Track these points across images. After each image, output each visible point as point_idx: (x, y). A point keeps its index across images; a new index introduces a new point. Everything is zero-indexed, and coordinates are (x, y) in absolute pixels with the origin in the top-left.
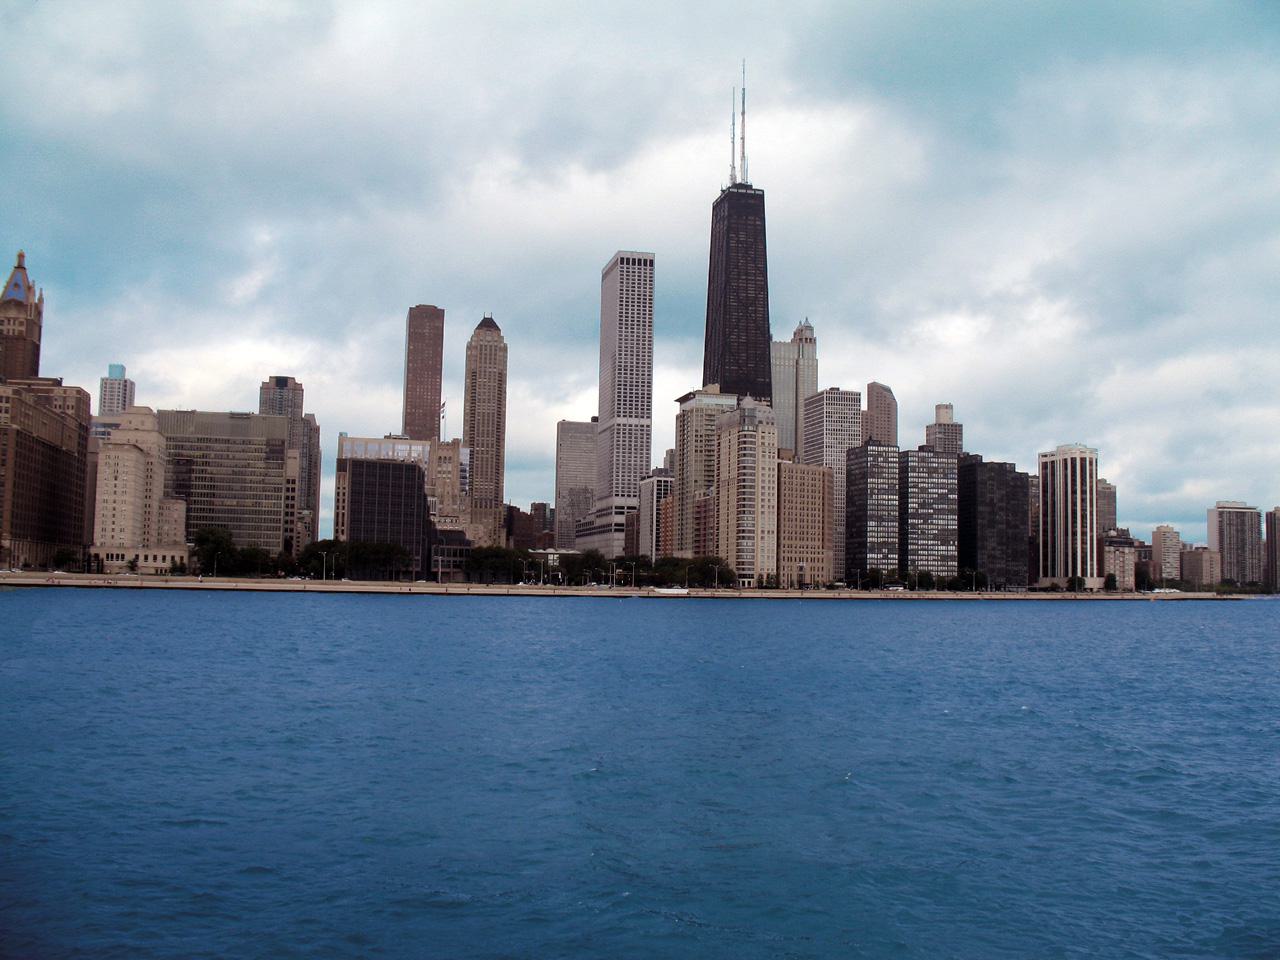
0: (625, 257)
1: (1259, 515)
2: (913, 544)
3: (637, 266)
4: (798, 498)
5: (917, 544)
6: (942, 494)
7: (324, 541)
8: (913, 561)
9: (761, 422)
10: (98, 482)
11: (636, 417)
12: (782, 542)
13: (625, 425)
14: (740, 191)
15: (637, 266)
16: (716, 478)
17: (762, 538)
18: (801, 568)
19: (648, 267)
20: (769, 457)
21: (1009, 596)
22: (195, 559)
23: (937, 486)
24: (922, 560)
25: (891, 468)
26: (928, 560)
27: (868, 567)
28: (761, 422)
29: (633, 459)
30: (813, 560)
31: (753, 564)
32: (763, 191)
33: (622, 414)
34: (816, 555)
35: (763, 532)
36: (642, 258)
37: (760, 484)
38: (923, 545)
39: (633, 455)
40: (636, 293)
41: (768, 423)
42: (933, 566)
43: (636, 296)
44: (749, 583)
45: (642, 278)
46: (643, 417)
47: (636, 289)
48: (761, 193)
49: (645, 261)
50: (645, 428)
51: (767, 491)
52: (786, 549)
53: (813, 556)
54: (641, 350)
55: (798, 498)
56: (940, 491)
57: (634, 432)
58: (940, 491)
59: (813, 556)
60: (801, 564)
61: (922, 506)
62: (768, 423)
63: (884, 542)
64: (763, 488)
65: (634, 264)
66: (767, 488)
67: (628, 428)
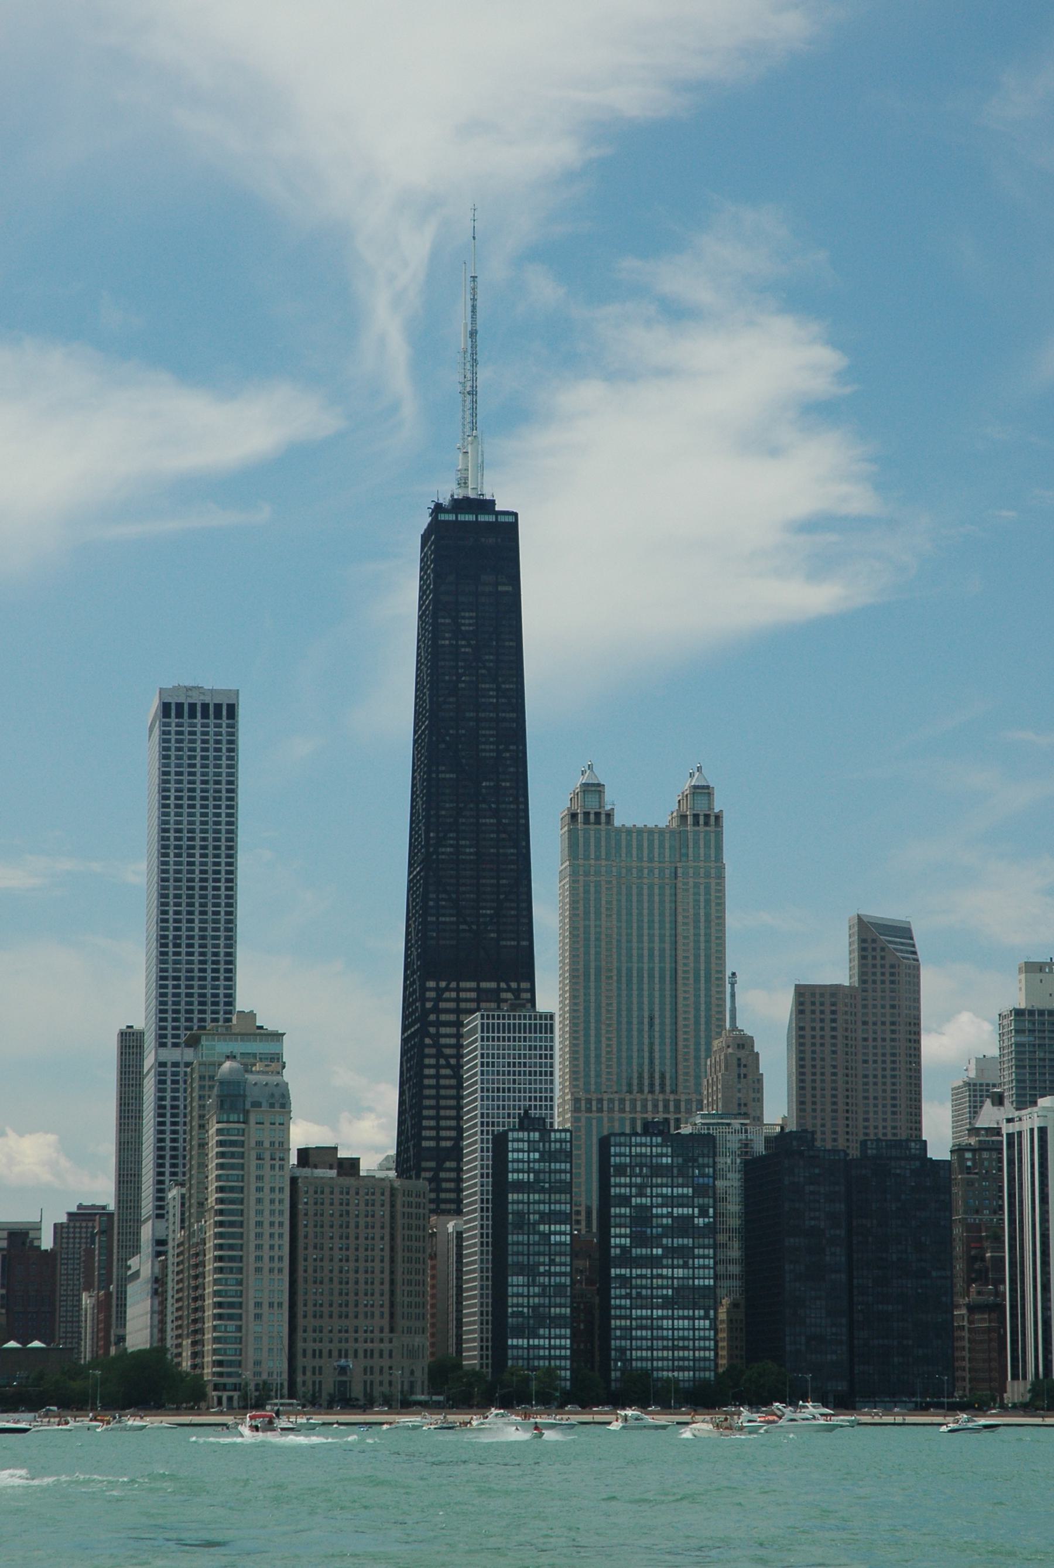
0: (173, 700)
2: (620, 1317)
3: (199, 720)
4: (336, 1240)
5: (630, 1318)
7: (791, 1132)
8: (622, 1350)
9: (257, 1104)
11: (175, 1045)
12: (301, 1322)
13: (175, 1064)
14: (462, 517)
15: (199, 720)
17: (258, 1316)
18: (343, 1370)
19: (224, 722)
20: (273, 1167)
21: (1038, 1421)
22: (618, 1251)
23: (671, 1201)
24: (638, 1349)
25: (556, 1171)
26: (652, 1349)
28: (257, 1104)
30: (369, 1354)
31: (239, 1364)
32: (516, 515)
33: (170, 1041)
34: (376, 1345)
35: (258, 1305)
36: (197, 699)
37: (253, 1219)
38: (641, 1318)
40: (198, 778)
41: (272, 1105)
42: (663, 1359)
44: (230, 1399)
45: (211, 745)
47: (198, 770)
48: (511, 519)
49: (218, 707)
51: (267, 1230)
52: (310, 1334)
53: (369, 1345)
54: (210, 901)
55: (336, 1240)
56: (677, 1211)
58: (677, 1211)
59: (369, 1345)
60: (343, 1362)
61: (639, 1240)
62: (272, 1105)
64: (259, 1224)
66: (266, 1224)
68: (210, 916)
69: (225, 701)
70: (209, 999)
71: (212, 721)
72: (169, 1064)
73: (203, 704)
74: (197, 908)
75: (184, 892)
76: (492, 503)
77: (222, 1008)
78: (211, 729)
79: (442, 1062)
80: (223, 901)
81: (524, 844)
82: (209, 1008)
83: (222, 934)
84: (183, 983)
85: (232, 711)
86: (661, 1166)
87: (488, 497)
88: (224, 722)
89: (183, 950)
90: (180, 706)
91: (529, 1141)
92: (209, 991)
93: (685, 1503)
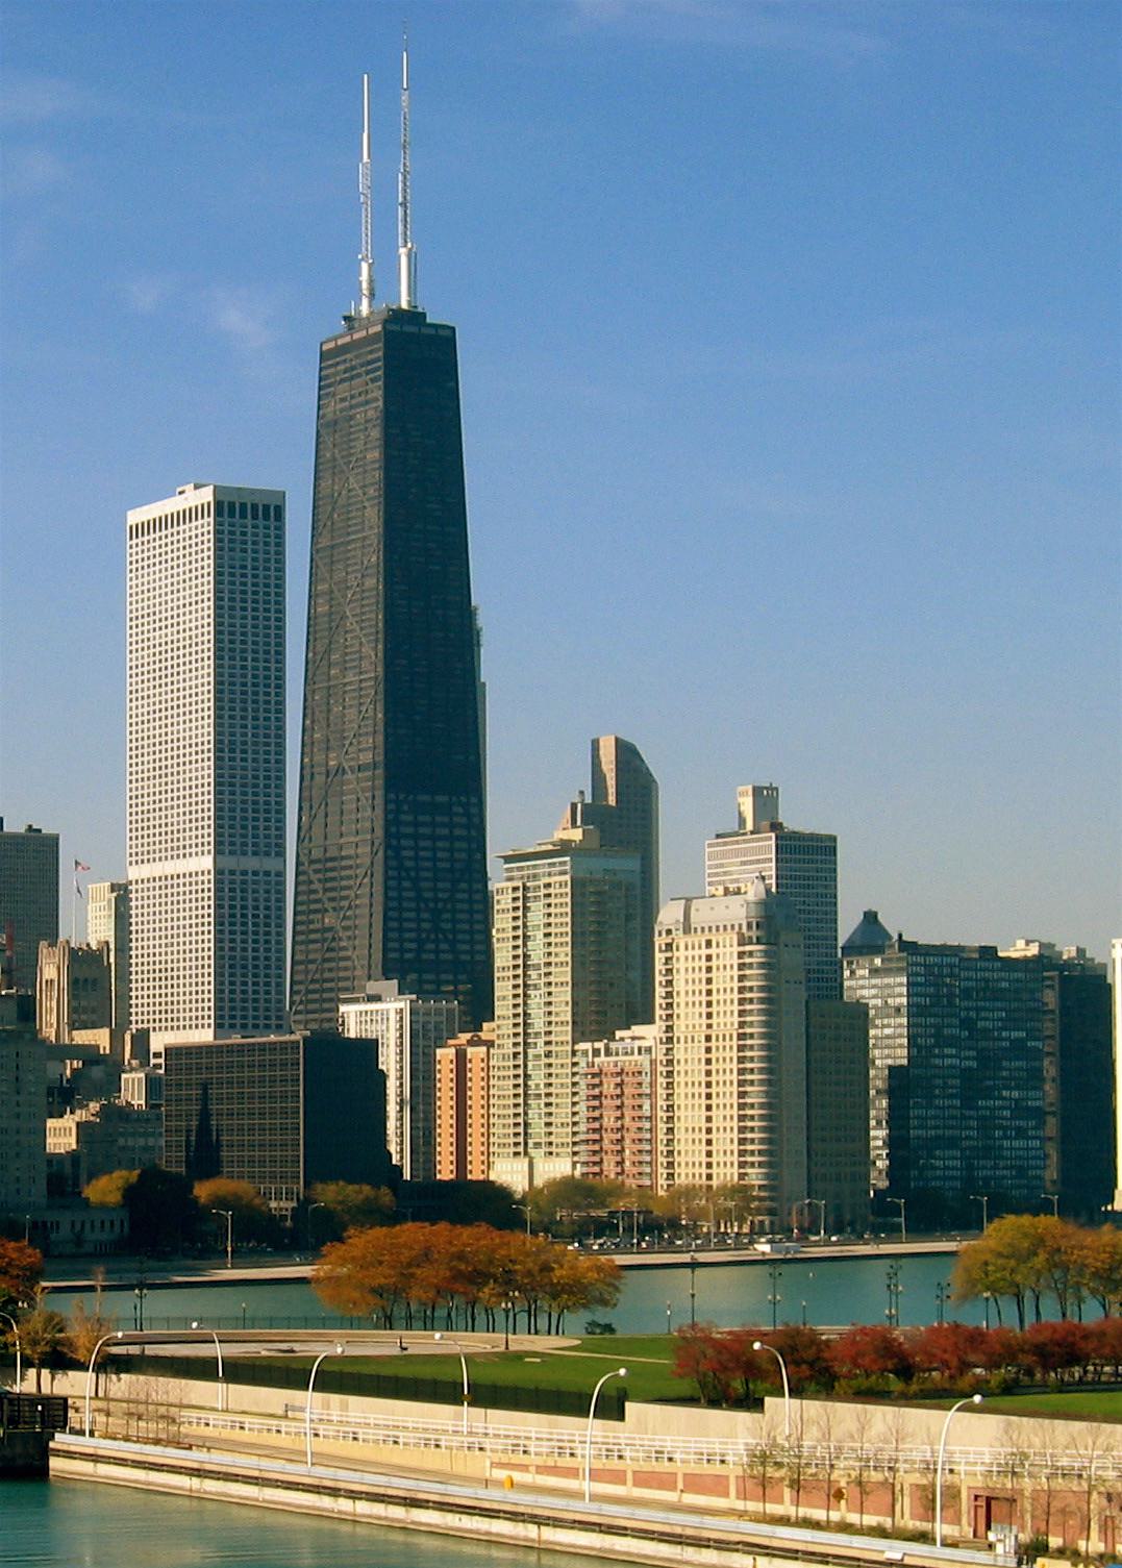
0: (226, 499)
1: (594, 1416)
3: (249, 521)
6: (1017, 1039)
10: (138, 509)
11: (255, 854)
16: (798, 843)
19: (272, 523)
27: (912, 1184)
29: (250, 946)
32: (453, 329)
36: (261, 501)
39: (251, 937)
43: (249, 588)
46: (267, 854)
48: (447, 333)
49: (266, 508)
50: (273, 878)
54: (262, 707)
57: (250, 887)
63: (938, 1137)
65: (243, 515)
67: (238, 878)
68: (261, 722)
69: (273, 503)
70: (262, 807)
71: (261, 522)
72: (226, 872)
73: (229, 503)
74: (250, 714)
75: (238, 696)
76: (424, 315)
77: (273, 815)
78: (261, 531)
79: (404, 874)
80: (273, 707)
81: (469, 658)
82: (262, 816)
83: (272, 740)
84: (238, 790)
85: (279, 512)
86: (1002, 990)
87: (420, 310)
88: (272, 523)
89: (238, 755)
90: (232, 505)
91: (925, 966)
92: (262, 799)
93: (1082, 1306)
